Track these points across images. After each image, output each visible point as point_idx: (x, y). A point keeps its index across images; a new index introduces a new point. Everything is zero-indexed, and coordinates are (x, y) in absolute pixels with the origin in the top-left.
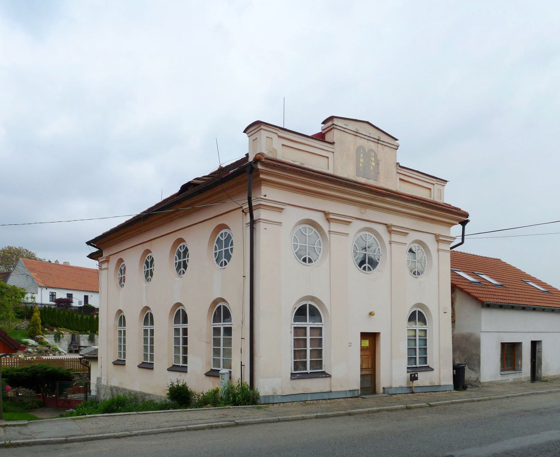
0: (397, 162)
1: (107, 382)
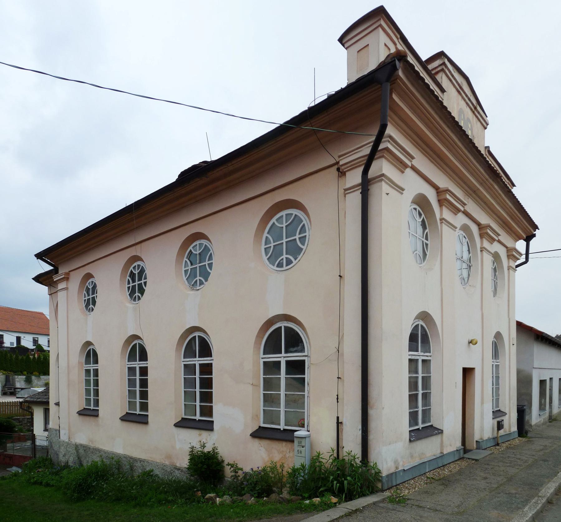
1: (69, 438)
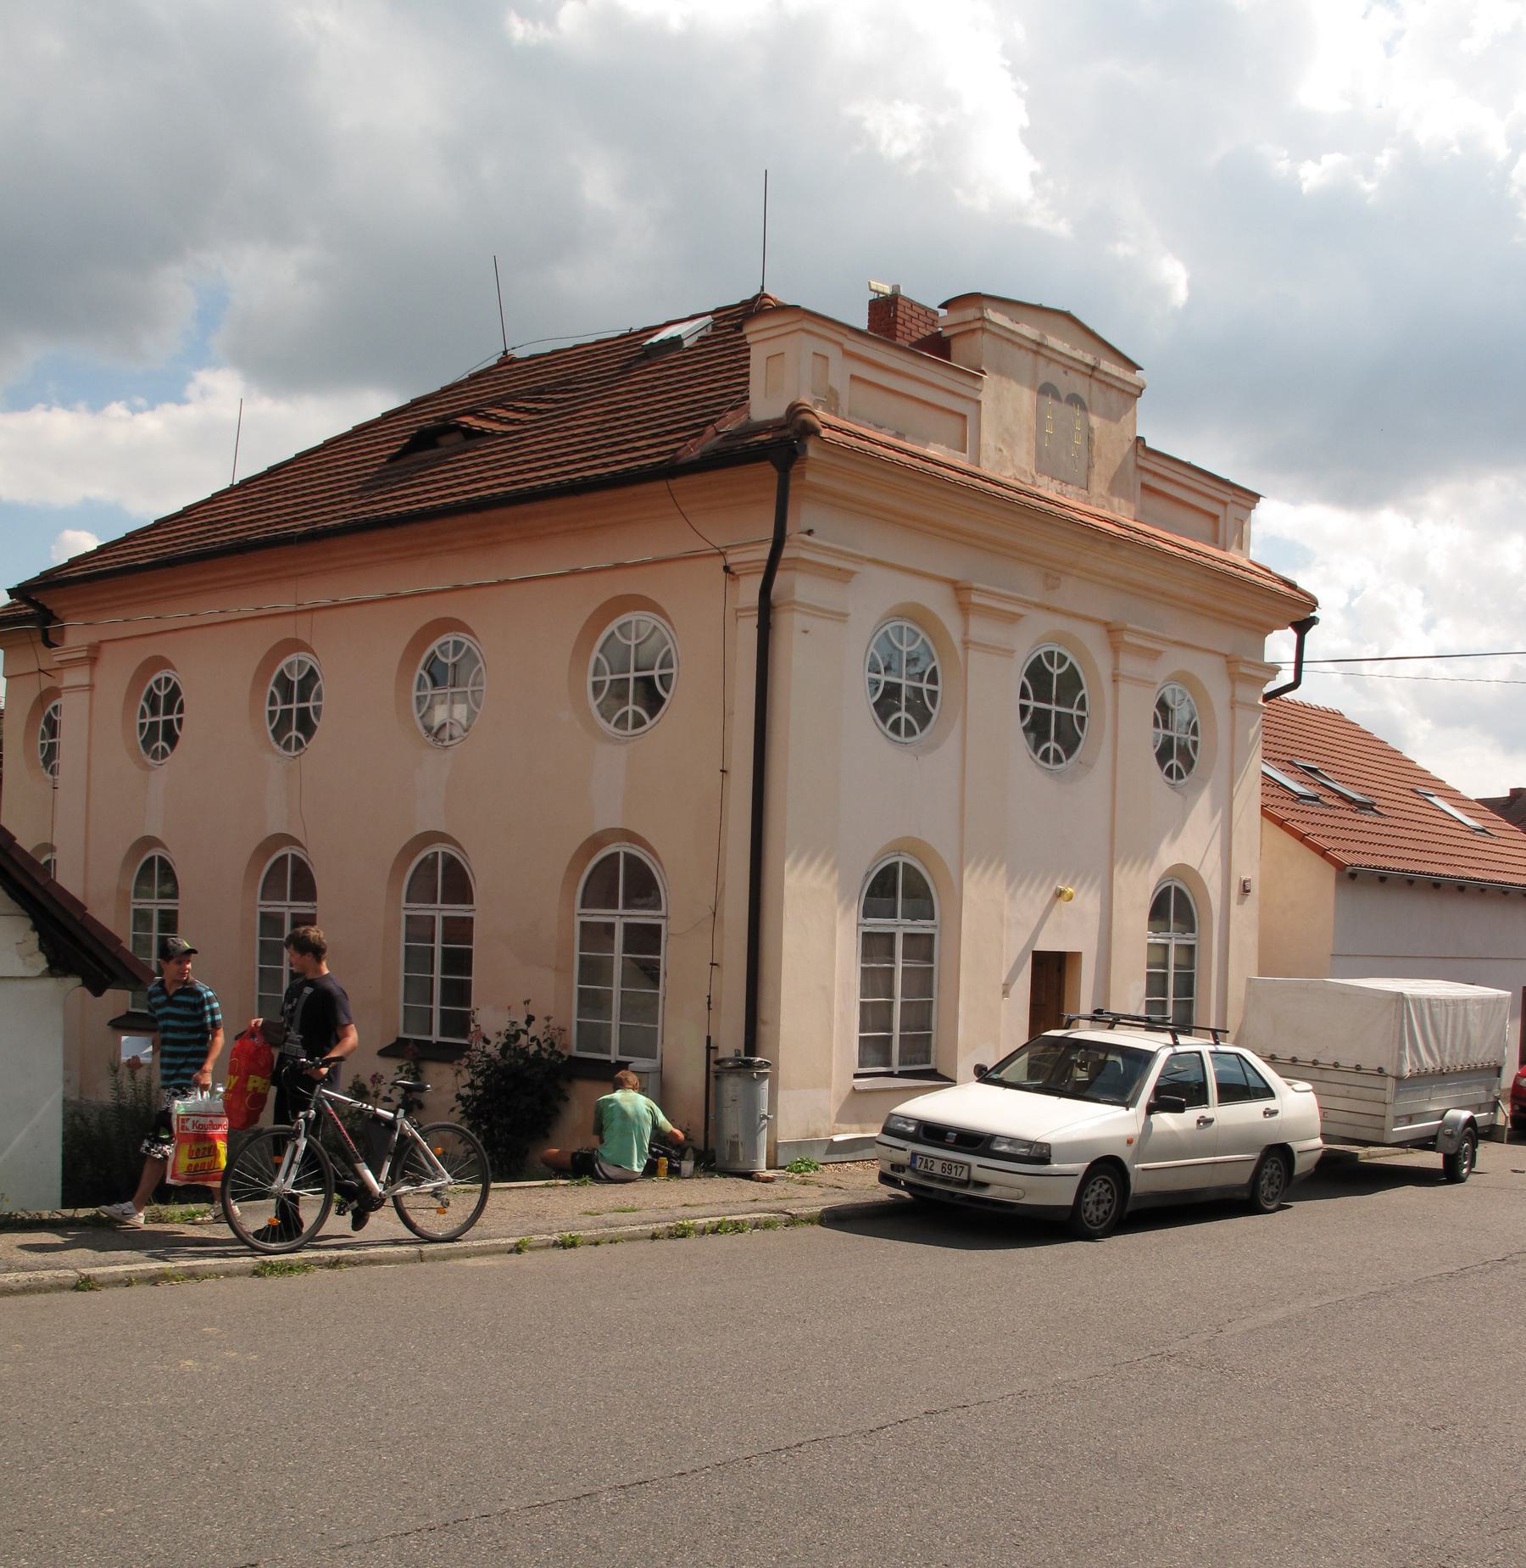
0: (1138, 435)
